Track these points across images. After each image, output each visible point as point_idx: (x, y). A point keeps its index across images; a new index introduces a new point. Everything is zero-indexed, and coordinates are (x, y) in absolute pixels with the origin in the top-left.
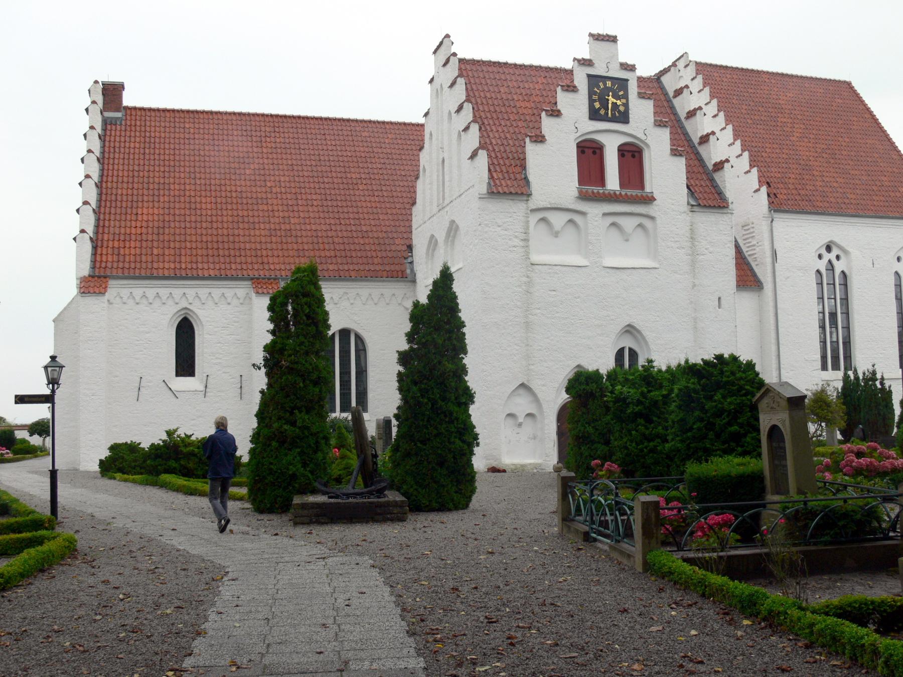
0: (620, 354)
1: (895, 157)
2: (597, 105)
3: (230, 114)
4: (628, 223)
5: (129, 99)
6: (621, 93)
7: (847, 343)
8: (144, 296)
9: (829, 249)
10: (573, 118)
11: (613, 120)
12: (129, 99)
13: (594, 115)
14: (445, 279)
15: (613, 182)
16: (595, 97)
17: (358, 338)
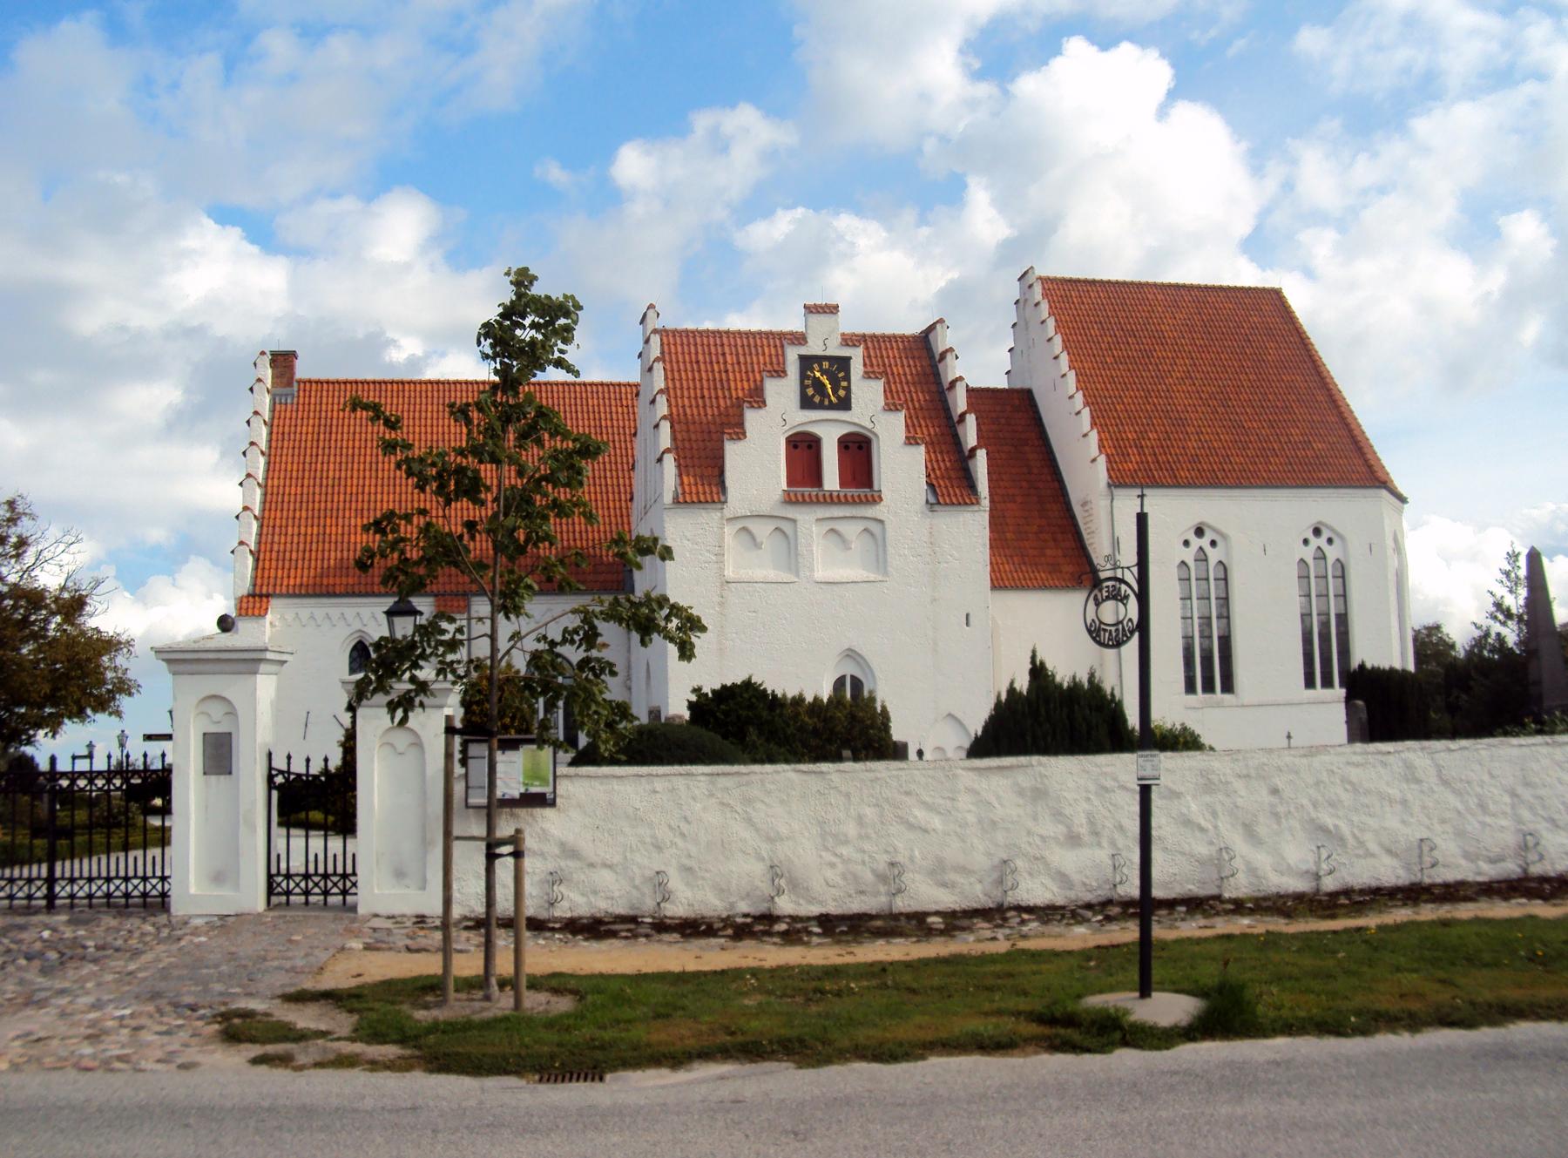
0: (839, 683)
1: (1320, 398)
2: (810, 391)
4: (851, 530)
6: (158, 802)
8: (312, 617)
9: (1199, 532)
10: (779, 411)
11: (832, 407)
12: (304, 370)
13: (806, 403)
15: (831, 478)
16: (844, 384)
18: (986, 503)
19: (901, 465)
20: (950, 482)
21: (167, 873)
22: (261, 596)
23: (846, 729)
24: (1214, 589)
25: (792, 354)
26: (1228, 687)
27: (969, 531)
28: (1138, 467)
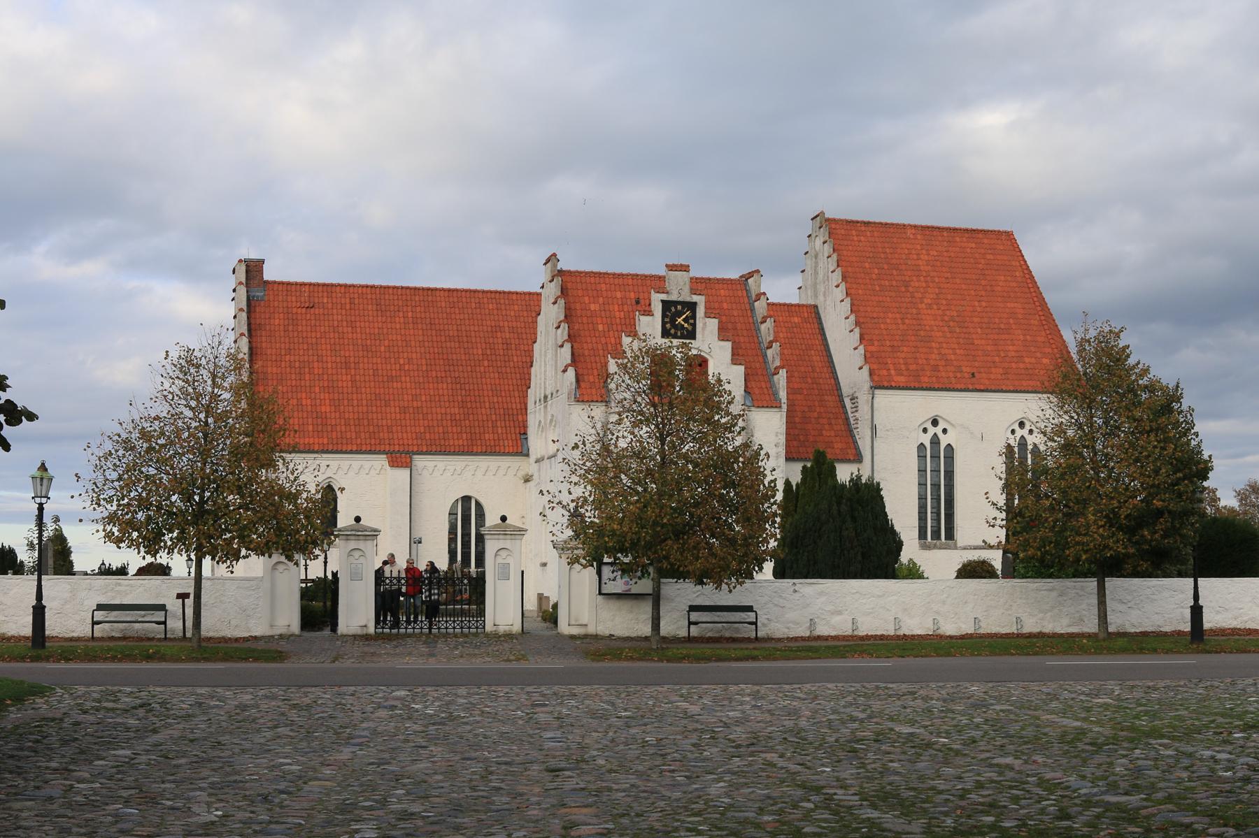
2: (668, 326)
3: (363, 286)
5: (268, 275)
9: (1022, 425)
12: (268, 275)
13: (665, 334)
14: (914, 573)
17: (478, 504)
18: (785, 407)
21: (416, 535)
22: (408, 452)
24: (938, 466)
25: (657, 299)
26: (950, 535)
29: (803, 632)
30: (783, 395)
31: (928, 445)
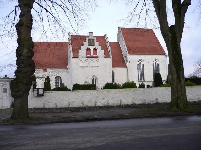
7: (143, 74)
9: (155, 60)
17: (60, 77)
19: (100, 52)
20: (107, 55)
23: (92, 87)
25: (87, 38)
27: (109, 61)
28: (132, 51)
29: (54, 106)
30: (111, 56)
31: (139, 64)
